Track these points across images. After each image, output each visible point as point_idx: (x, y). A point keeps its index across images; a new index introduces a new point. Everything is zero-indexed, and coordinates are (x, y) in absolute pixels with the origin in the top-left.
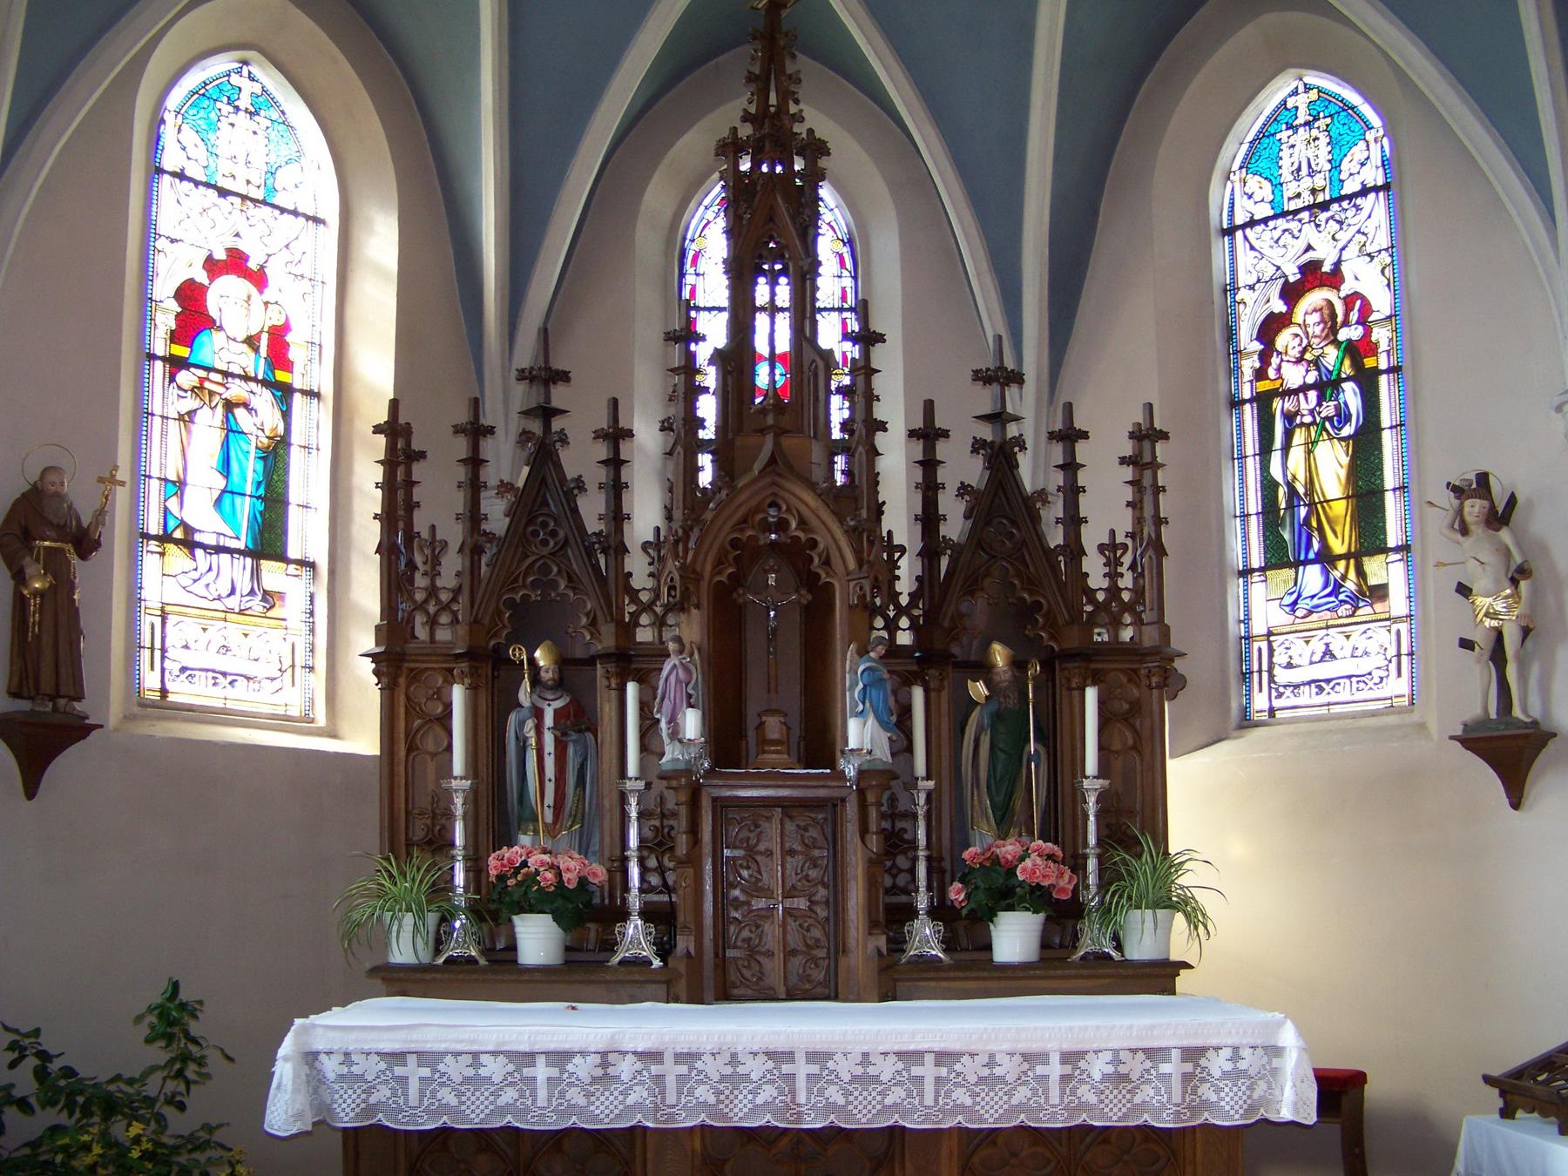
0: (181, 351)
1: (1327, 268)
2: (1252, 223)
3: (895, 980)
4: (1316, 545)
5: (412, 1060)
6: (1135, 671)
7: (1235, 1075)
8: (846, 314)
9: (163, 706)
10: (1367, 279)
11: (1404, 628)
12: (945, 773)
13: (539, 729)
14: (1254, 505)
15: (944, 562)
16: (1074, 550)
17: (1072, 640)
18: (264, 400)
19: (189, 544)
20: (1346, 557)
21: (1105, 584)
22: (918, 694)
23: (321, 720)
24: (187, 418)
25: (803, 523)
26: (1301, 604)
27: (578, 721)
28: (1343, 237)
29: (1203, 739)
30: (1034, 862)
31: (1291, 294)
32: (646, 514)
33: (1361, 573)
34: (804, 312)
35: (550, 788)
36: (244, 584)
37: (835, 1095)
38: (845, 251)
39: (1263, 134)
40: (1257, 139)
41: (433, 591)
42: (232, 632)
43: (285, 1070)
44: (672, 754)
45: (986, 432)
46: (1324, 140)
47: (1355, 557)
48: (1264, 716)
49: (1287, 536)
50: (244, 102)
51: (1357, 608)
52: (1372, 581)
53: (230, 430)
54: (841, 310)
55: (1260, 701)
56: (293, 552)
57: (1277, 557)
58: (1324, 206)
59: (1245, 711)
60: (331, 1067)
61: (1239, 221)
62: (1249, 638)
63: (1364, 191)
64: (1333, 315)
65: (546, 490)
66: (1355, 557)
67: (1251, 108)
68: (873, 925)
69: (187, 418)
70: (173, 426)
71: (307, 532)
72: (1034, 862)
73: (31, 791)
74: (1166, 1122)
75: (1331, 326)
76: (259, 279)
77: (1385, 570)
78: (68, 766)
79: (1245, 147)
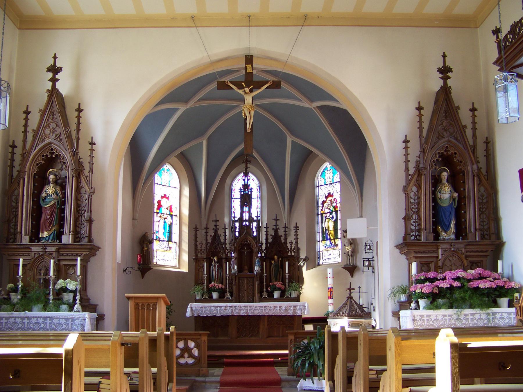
0: (158, 211)
3: (261, 300)
7: (300, 309)
9: (156, 265)
12: (480, 243)
14: (320, 231)
18: (169, 217)
19: (159, 240)
22: (264, 263)
23: (178, 267)
24: (159, 221)
27: (220, 267)
30: (278, 284)
31: (326, 197)
34: (250, 212)
36: (167, 246)
37: (252, 311)
38: (258, 188)
39: (323, 171)
41: (291, 248)
42: (165, 253)
43: (189, 309)
44: (233, 271)
45: (274, 227)
47: (334, 239)
50: (166, 171)
53: (165, 222)
55: (321, 262)
56: (173, 241)
57: (324, 239)
58: (331, 184)
59: (318, 263)
60: (194, 309)
63: (337, 182)
65: (216, 237)
66: (334, 239)
68: (258, 293)
69: (159, 221)
70: (157, 223)
71: (175, 237)
72: (278, 284)
73: (143, 277)
74: (291, 315)
75: (332, 203)
76: (168, 198)
77: (338, 241)
78: (147, 274)
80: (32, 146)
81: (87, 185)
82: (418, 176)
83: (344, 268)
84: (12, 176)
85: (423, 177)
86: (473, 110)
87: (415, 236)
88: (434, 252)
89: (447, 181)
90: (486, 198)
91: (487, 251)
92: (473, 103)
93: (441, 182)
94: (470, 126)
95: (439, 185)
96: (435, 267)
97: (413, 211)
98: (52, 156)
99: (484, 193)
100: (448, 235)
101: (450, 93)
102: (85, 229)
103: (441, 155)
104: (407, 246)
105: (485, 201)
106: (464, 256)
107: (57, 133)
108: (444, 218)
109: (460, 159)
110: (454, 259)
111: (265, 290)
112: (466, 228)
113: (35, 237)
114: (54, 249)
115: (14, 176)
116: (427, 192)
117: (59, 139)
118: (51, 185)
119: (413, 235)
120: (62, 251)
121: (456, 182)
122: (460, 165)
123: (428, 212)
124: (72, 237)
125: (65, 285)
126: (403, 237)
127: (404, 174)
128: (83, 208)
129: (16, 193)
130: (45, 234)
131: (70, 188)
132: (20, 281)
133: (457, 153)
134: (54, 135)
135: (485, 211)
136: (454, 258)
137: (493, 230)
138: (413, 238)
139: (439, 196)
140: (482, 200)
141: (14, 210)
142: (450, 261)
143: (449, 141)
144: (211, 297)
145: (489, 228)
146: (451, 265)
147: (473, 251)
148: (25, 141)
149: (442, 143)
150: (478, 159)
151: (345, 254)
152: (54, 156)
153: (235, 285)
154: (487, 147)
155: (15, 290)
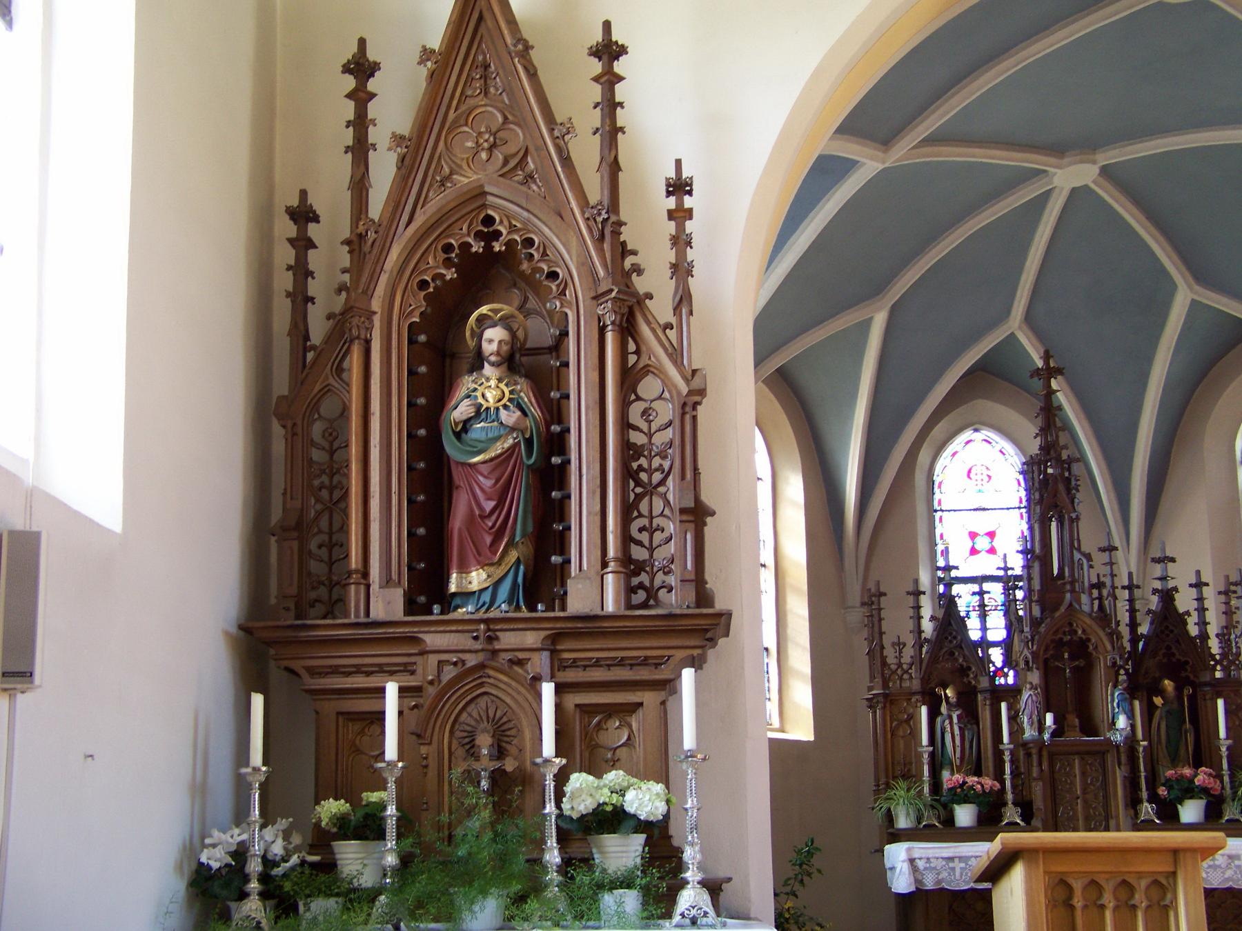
5: (957, 860)
13: (951, 723)
15: (1141, 644)
16: (1204, 636)
21: (895, 661)
32: (997, 628)
35: (958, 750)
38: (1021, 478)
41: (900, 665)
45: (1158, 585)
60: (921, 864)
68: (1126, 806)
80: (396, 203)
81: (675, 363)
84: (307, 338)
98: (488, 247)
102: (671, 543)
107: (511, 148)
111: (1145, 795)
113: (428, 588)
114: (531, 639)
115: (316, 337)
117: (520, 175)
118: (488, 370)
120: (571, 650)
124: (616, 582)
125: (615, 799)
128: (656, 462)
129: (328, 407)
130: (477, 579)
131: (588, 375)
132: (1010, 805)
134: (499, 156)
141: (325, 479)
144: (949, 821)
148: (360, 187)
152: (497, 247)
153: (1039, 778)
155: (368, 827)
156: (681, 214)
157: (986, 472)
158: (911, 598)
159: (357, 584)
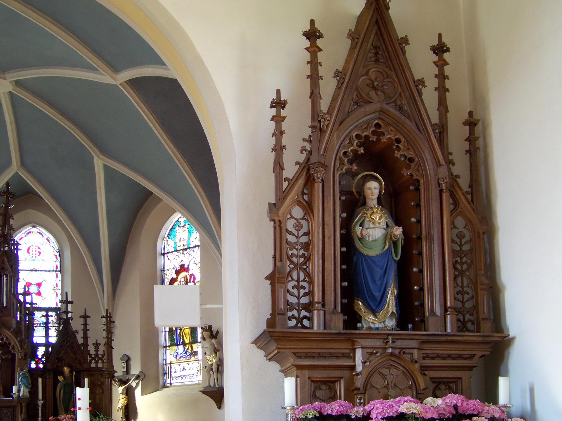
1: (186, 266)
2: (169, 252)
4: (182, 340)
6: (102, 374)
8: (57, 272)
10: (195, 270)
11: (201, 362)
16: (86, 345)
17: (86, 366)
20: (188, 344)
21: (95, 353)
25: (7, 339)
26: (178, 356)
28: (190, 258)
29: (151, 391)
31: (178, 272)
33: (192, 348)
38: (58, 254)
39: (173, 228)
40: (171, 229)
41: (97, 355)
46: (187, 231)
48: (169, 385)
49: (175, 338)
51: (191, 357)
52: (195, 350)
54: (56, 271)
55: (168, 381)
57: (174, 343)
58: (186, 249)
61: (166, 252)
62: (166, 364)
63: (195, 246)
64: (187, 279)
67: (169, 221)
77: (197, 348)
79: (168, 231)
82: (306, 184)
83: (204, 392)
85: (318, 186)
86: (440, 49)
87: (299, 320)
88: (344, 356)
89: (379, 203)
90: (471, 240)
91: (471, 357)
92: (440, 36)
93: (364, 203)
94: (432, 83)
95: (358, 210)
96: (346, 390)
97: (292, 262)
99: (466, 232)
100: (381, 320)
101: (388, 8)
103: (365, 142)
104: (278, 338)
105: (466, 248)
106: (417, 366)
108: (369, 279)
109: (411, 154)
110: (394, 374)
112: (422, 305)
116: (329, 219)
119: (293, 317)
121: (397, 204)
122: (408, 168)
123: (329, 266)
126: (268, 320)
127: (272, 178)
133: (403, 140)
135: (468, 269)
136: (394, 371)
137: (485, 310)
138: (293, 323)
139: (359, 233)
140: (461, 246)
142: (384, 376)
143: (382, 111)
145: (476, 307)
146: (386, 387)
147: (438, 357)
149: (365, 116)
150: (450, 157)
151: (208, 369)
154: (471, 132)
156: (280, 119)
157: (38, 250)
158: (82, 319)
159: (318, 310)
